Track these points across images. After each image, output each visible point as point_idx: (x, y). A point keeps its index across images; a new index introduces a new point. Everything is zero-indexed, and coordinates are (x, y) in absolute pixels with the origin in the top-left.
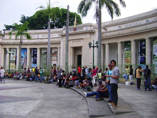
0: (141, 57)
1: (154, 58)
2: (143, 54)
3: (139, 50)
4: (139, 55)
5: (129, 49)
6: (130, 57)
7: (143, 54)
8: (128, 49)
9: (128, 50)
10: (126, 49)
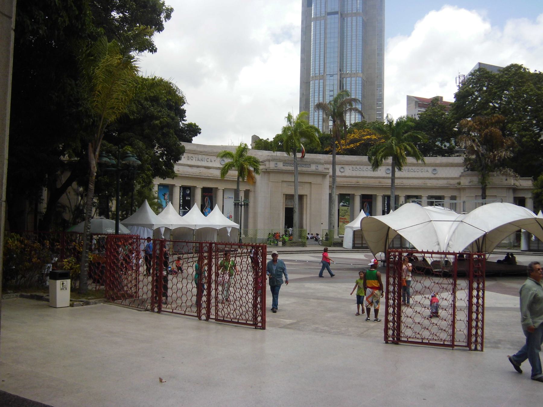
2: (186, 207)
3: (181, 201)
4: (181, 208)
5: (348, 205)
6: (348, 216)
7: (186, 207)
8: (345, 204)
9: (345, 206)
10: (341, 204)
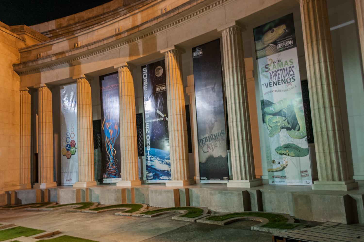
0: (153, 122)
1: (268, 117)
